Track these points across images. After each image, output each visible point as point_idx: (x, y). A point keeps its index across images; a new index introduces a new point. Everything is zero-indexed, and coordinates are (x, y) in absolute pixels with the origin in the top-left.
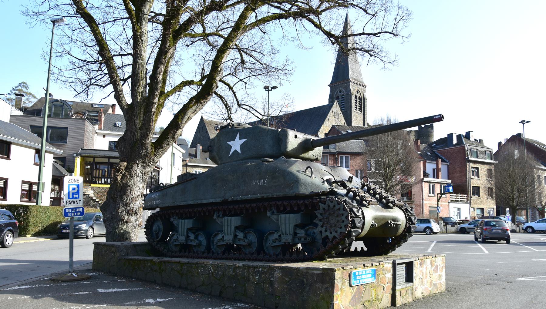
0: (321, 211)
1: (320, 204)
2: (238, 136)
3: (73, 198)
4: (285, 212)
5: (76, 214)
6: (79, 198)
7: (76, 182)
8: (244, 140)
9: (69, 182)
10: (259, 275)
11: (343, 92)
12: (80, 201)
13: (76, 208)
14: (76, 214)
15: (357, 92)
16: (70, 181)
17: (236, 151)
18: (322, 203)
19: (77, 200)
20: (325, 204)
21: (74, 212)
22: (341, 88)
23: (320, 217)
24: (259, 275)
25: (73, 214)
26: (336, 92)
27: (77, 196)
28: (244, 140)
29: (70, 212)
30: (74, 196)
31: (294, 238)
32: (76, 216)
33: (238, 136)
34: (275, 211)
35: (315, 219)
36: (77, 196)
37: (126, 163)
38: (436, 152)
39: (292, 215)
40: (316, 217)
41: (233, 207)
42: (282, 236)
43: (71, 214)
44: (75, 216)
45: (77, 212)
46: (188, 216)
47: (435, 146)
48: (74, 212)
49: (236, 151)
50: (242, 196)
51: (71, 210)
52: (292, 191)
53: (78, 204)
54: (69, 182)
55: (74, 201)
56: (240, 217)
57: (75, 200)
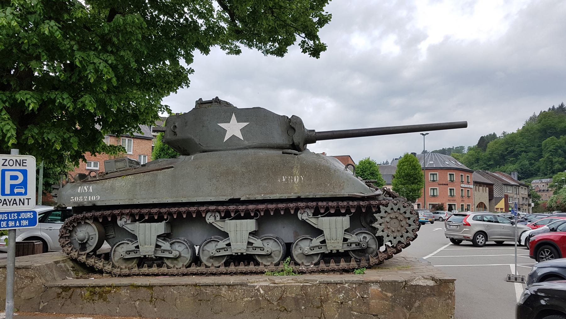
1: (381, 206)
3: (12, 193)
5: (20, 223)
6: (26, 193)
7: (20, 165)
8: (221, 125)
9: (3, 165)
10: (344, 292)
12: (28, 199)
13: (19, 213)
14: (20, 223)
16: (6, 163)
18: (383, 205)
19: (22, 197)
21: (15, 221)
23: (380, 221)
24: (344, 292)
25: (11, 224)
27: (23, 191)
28: (221, 125)
29: (4, 220)
30: (16, 191)
32: (18, 226)
36: (23, 191)
37: (33, 142)
40: (376, 220)
43: (7, 224)
44: (15, 226)
45: (22, 219)
48: (15, 221)
50: (265, 194)
51: (8, 216)
52: (343, 191)
53: (23, 204)
54: (3, 165)
55: (15, 200)
57: (17, 198)
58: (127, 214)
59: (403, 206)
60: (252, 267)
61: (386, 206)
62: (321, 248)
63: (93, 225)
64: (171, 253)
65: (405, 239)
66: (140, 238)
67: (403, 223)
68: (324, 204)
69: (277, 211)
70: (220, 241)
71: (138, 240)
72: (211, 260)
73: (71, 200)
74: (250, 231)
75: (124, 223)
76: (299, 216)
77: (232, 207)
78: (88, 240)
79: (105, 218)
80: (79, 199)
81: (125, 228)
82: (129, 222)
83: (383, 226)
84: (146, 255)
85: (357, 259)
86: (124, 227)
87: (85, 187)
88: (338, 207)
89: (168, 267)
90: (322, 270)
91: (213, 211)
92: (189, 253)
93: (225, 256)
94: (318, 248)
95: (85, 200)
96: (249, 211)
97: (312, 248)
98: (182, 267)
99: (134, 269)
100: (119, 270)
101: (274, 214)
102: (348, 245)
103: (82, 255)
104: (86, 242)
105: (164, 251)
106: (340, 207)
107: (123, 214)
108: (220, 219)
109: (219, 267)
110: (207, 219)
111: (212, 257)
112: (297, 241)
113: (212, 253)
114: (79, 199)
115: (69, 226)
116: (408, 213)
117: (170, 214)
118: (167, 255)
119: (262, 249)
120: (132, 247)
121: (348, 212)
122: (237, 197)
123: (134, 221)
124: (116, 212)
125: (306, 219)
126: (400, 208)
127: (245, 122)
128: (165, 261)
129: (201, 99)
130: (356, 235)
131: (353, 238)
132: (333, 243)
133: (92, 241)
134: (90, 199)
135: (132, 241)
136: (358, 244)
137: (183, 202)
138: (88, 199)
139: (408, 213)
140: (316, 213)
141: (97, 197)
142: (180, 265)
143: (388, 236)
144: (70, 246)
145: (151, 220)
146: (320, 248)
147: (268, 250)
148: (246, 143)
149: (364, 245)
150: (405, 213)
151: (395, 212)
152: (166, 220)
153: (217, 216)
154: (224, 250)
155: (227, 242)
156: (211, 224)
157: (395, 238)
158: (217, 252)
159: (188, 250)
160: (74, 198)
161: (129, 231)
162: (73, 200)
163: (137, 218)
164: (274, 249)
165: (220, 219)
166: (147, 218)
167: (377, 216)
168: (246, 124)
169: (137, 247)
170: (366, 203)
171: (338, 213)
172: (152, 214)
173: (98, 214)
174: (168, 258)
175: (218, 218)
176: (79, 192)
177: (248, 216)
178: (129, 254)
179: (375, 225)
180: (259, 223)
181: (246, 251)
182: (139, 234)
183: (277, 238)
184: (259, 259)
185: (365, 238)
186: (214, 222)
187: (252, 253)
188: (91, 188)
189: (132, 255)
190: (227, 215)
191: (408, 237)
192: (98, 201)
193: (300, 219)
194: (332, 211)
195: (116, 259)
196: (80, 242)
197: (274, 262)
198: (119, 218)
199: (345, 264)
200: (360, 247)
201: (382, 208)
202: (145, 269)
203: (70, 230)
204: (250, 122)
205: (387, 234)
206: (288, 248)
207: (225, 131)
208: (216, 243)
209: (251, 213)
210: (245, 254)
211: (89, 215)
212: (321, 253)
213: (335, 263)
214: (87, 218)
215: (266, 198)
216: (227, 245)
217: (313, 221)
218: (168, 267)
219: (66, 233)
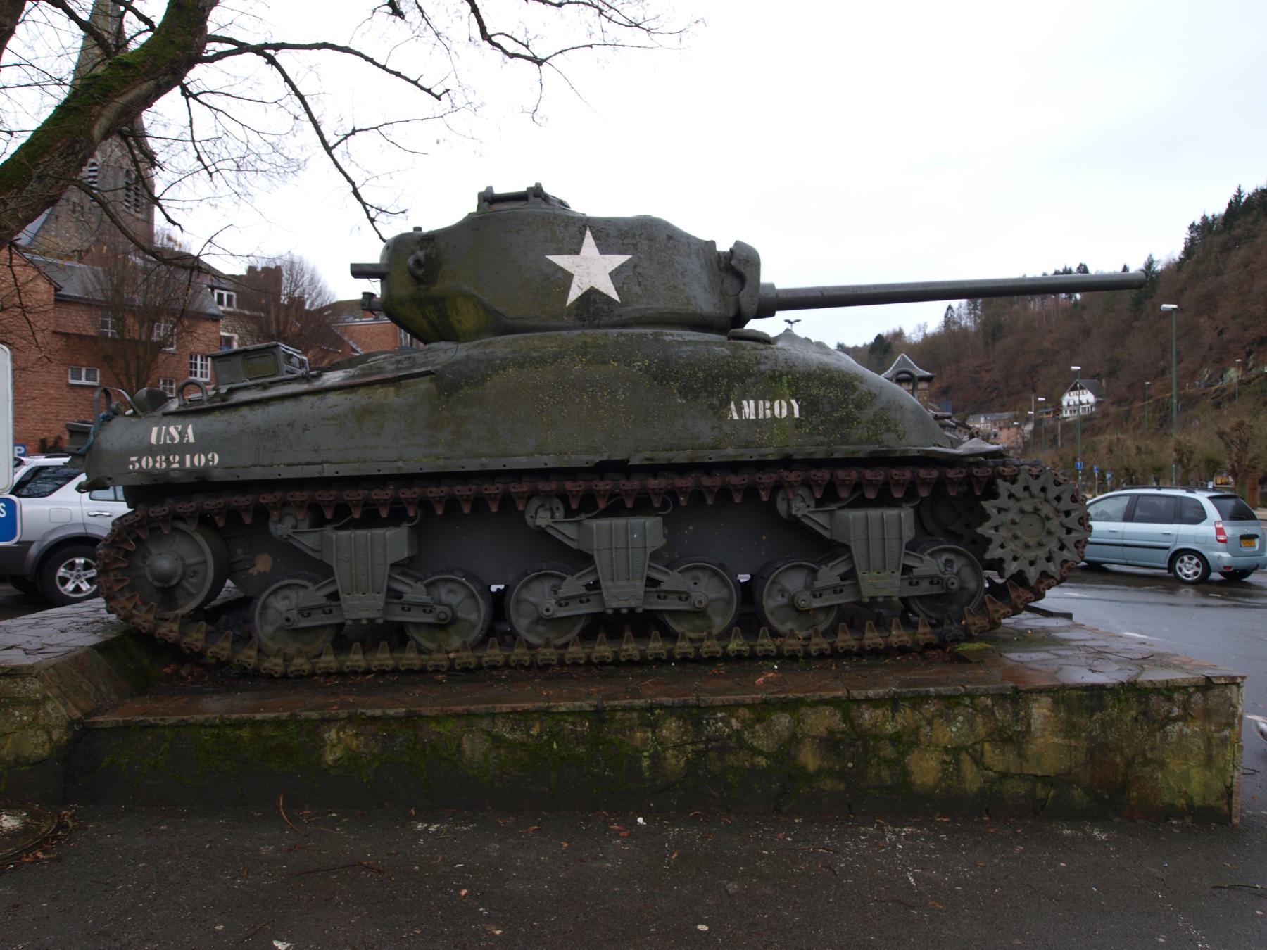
0: (1002, 501)
1: (1000, 481)
18: (1005, 479)
58: (300, 506)
59: (1055, 481)
60: (656, 646)
61: (1013, 480)
62: (841, 591)
63: (200, 539)
64: (431, 612)
65: (1059, 565)
66: (342, 573)
67: (1053, 525)
68: (854, 475)
69: (452, 504)
70: (569, 578)
71: (337, 576)
72: (541, 629)
73: (131, 467)
74: (392, 562)
75: (290, 531)
76: (781, 507)
77: (603, 485)
78: (183, 577)
79: (233, 516)
80: (155, 462)
81: (296, 544)
82: (304, 526)
83: (1003, 533)
84: (360, 620)
85: (931, 618)
86: (291, 541)
87: (172, 430)
88: (886, 483)
89: (421, 651)
90: (323, 673)
91: (548, 495)
92: (478, 610)
93: (580, 616)
94: (831, 591)
95: (176, 466)
96: (402, 503)
97: (563, 602)
98: (708, 639)
99: (324, 658)
100: (279, 661)
101: (634, 504)
102: (911, 584)
103: (166, 620)
104: (178, 584)
105: (408, 607)
106: (623, 493)
107: (286, 504)
108: (565, 517)
109: (566, 646)
110: (527, 518)
111: (540, 620)
112: (774, 575)
113: (548, 610)
114: (155, 462)
115: (125, 541)
116: (1066, 497)
117: (425, 505)
118: (673, 604)
119: (428, 609)
120: (315, 595)
121: (910, 494)
122: (618, 456)
123: (319, 522)
124: (267, 499)
125: (548, 526)
126: (1046, 485)
127: (621, 253)
128: (412, 632)
129: (490, 189)
130: (931, 555)
131: (927, 565)
132: (877, 578)
133: (193, 580)
134: (188, 464)
135: (315, 582)
136: (933, 580)
137: (241, 479)
138: (182, 462)
139: (1066, 497)
140: (829, 496)
141: (210, 456)
142: (456, 642)
143: (1015, 559)
144: (128, 595)
145: (371, 519)
146: (581, 599)
147: (702, 599)
148: (626, 312)
149: (953, 584)
150: (1058, 498)
151: (1032, 496)
152: (411, 519)
153: (558, 509)
154: (578, 600)
155: (330, 589)
156: (541, 532)
157: (1032, 563)
158: (303, 616)
159: (477, 602)
160: (139, 461)
161: (309, 552)
162: (137, 465)
163: (329, 515)
164: (713, 596)
165: (565, 517)
166: (602, 505)
167: (990, 506)
168: (623, 259)
169: (334, 596)
170: (961, 472)
171: (884, 499)
172: (374, 504)
173: (212, 504)
174: (418, 625)
175: (559, 515)
176: (153, 440)
177: (643, 506)
178: (821, 595)
179: (985, 530)
180: (419, 534)
181: (644, 603)
182: (337, 560)
183: (722, 566)
184: (676, 627)
185: (949, 563)
186: (553, 525)
187: (656, 608)
188: (190, 430)
189: (318, 620)
190: (588, 505)
191: (1065, 561)
192: (215, 467)
193: (532, 527)
194: (871, 495)
195: (269, 629)
196: (157, 584)
197: (715, 631)
198: (275, 515)
199: (902, 632)
200: (943, 588)
201: (1003, 486)
202: (356, 657)
203: (127, 551)
204: (633, 254)
205: (1013, 554)
206: (499, 604)
207: (569, 277)
208: (553, 582)
209: (653, 498)
210: (380, 621)
211: (184, 507)
212: (587, 615)
213: (391, 652)
214: (180, 518)
215: (698, 461)
216: (588, 587)
217: (819, 520)
218: (421, 651)
219: (116, 560)
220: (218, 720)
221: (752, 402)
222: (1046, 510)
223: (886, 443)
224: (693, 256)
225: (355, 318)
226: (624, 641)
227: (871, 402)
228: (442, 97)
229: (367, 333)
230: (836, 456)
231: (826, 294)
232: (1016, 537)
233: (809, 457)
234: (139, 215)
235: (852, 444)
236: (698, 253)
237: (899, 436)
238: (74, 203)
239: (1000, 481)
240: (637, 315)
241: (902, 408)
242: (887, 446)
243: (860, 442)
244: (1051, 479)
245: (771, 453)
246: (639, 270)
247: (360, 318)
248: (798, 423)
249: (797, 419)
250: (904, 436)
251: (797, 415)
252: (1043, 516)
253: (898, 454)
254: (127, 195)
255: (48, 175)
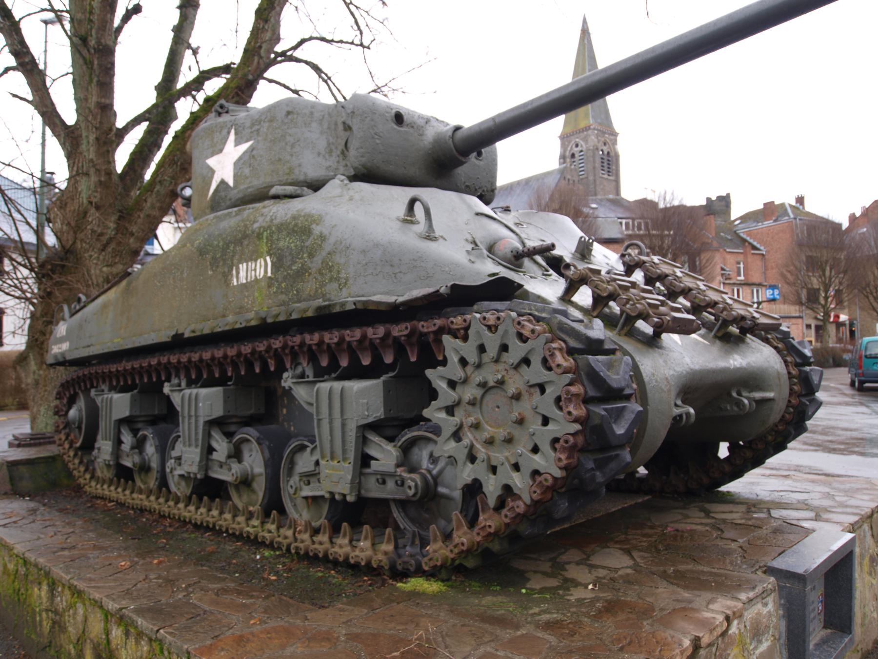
0: (454, 370)
1: (447, 339)
2: (232, 137)
4: (333, 371)
11: (582, 146)
15: (605, 144)
17: (223, 182)
20: (465, 338)
22: (577, 140)
26: (570, 146)
31: (361, 474)
33: (232, 137)
34: (309, 372)
35: (428, 405)
38: (742, 235)
39: (355, 386)
40: (433, 394)
41: (169, 359)
42: (322, 462)
46: (217, 375)
47: (739, 224)
49: (223, 182)
56: (219, 389)
220: (61, 566)
221: (245, 264)
222: (490, 375)
223: (328, 296)
224: (314, 125)
225: (758, 222)
226: (341, 535)
227: (321, 246)
228: (370, 46)
229: (768, 234)
230: (294, 316)
231: (497, 121)
232: (476, 426)
233: (248, 325)
234: (611, 178)
235: (304, 300)
236: (321, 120)
237: (340, 285)
238: (569, 180)
239: (447, 339)
240: (240, 195)
241: (377, 245)
242: (329, 300)
243: (310, 298)
244: (512, 331)
245: (250, 318)
246: (254, 152)
247: (762, 222)
248: (270, 281)
249: (270, 278)
250: (346, 283)
251: (269, 274)
252: (495, 384)
253: (337, 309)
254: (602, 166)
255: (164, 180)
